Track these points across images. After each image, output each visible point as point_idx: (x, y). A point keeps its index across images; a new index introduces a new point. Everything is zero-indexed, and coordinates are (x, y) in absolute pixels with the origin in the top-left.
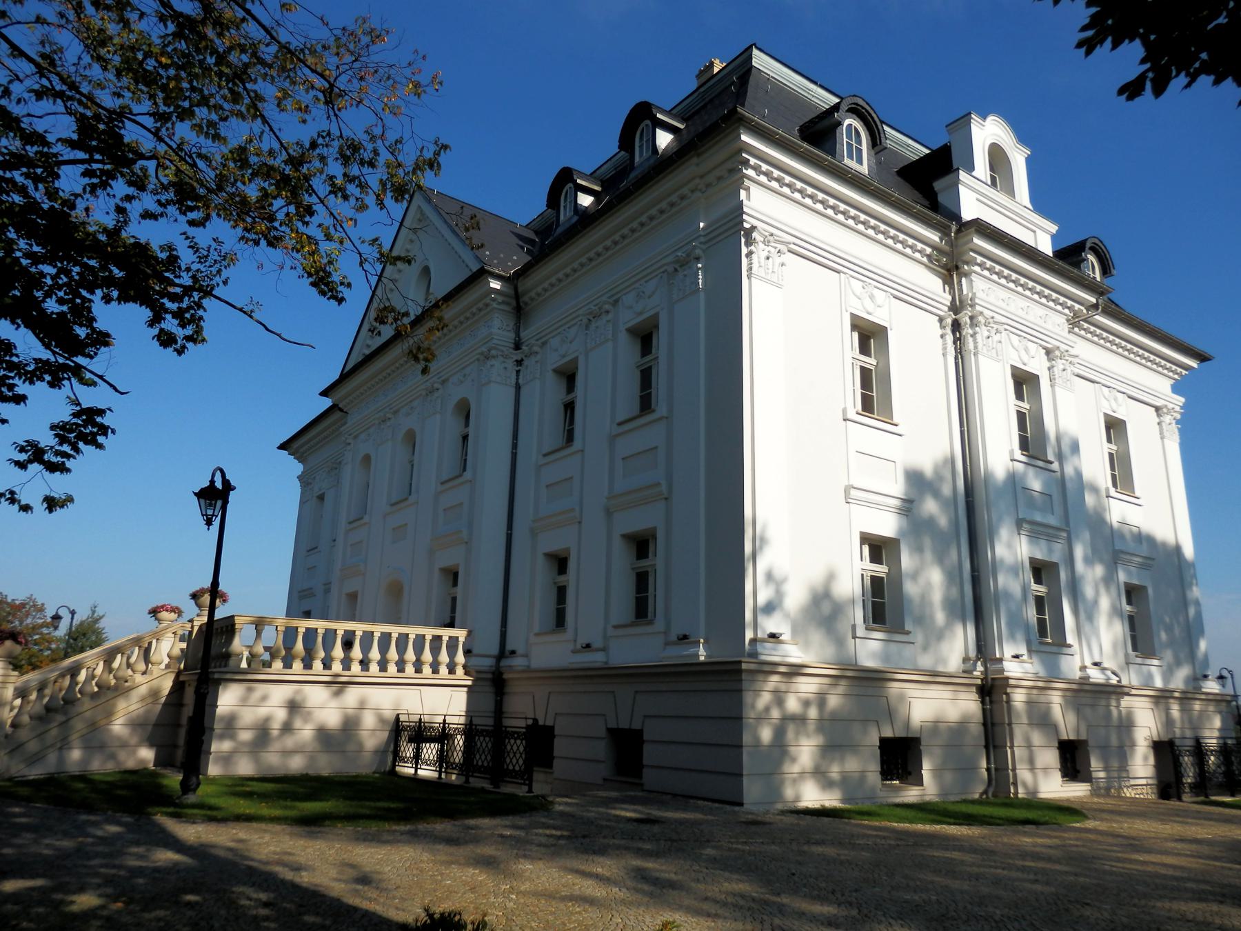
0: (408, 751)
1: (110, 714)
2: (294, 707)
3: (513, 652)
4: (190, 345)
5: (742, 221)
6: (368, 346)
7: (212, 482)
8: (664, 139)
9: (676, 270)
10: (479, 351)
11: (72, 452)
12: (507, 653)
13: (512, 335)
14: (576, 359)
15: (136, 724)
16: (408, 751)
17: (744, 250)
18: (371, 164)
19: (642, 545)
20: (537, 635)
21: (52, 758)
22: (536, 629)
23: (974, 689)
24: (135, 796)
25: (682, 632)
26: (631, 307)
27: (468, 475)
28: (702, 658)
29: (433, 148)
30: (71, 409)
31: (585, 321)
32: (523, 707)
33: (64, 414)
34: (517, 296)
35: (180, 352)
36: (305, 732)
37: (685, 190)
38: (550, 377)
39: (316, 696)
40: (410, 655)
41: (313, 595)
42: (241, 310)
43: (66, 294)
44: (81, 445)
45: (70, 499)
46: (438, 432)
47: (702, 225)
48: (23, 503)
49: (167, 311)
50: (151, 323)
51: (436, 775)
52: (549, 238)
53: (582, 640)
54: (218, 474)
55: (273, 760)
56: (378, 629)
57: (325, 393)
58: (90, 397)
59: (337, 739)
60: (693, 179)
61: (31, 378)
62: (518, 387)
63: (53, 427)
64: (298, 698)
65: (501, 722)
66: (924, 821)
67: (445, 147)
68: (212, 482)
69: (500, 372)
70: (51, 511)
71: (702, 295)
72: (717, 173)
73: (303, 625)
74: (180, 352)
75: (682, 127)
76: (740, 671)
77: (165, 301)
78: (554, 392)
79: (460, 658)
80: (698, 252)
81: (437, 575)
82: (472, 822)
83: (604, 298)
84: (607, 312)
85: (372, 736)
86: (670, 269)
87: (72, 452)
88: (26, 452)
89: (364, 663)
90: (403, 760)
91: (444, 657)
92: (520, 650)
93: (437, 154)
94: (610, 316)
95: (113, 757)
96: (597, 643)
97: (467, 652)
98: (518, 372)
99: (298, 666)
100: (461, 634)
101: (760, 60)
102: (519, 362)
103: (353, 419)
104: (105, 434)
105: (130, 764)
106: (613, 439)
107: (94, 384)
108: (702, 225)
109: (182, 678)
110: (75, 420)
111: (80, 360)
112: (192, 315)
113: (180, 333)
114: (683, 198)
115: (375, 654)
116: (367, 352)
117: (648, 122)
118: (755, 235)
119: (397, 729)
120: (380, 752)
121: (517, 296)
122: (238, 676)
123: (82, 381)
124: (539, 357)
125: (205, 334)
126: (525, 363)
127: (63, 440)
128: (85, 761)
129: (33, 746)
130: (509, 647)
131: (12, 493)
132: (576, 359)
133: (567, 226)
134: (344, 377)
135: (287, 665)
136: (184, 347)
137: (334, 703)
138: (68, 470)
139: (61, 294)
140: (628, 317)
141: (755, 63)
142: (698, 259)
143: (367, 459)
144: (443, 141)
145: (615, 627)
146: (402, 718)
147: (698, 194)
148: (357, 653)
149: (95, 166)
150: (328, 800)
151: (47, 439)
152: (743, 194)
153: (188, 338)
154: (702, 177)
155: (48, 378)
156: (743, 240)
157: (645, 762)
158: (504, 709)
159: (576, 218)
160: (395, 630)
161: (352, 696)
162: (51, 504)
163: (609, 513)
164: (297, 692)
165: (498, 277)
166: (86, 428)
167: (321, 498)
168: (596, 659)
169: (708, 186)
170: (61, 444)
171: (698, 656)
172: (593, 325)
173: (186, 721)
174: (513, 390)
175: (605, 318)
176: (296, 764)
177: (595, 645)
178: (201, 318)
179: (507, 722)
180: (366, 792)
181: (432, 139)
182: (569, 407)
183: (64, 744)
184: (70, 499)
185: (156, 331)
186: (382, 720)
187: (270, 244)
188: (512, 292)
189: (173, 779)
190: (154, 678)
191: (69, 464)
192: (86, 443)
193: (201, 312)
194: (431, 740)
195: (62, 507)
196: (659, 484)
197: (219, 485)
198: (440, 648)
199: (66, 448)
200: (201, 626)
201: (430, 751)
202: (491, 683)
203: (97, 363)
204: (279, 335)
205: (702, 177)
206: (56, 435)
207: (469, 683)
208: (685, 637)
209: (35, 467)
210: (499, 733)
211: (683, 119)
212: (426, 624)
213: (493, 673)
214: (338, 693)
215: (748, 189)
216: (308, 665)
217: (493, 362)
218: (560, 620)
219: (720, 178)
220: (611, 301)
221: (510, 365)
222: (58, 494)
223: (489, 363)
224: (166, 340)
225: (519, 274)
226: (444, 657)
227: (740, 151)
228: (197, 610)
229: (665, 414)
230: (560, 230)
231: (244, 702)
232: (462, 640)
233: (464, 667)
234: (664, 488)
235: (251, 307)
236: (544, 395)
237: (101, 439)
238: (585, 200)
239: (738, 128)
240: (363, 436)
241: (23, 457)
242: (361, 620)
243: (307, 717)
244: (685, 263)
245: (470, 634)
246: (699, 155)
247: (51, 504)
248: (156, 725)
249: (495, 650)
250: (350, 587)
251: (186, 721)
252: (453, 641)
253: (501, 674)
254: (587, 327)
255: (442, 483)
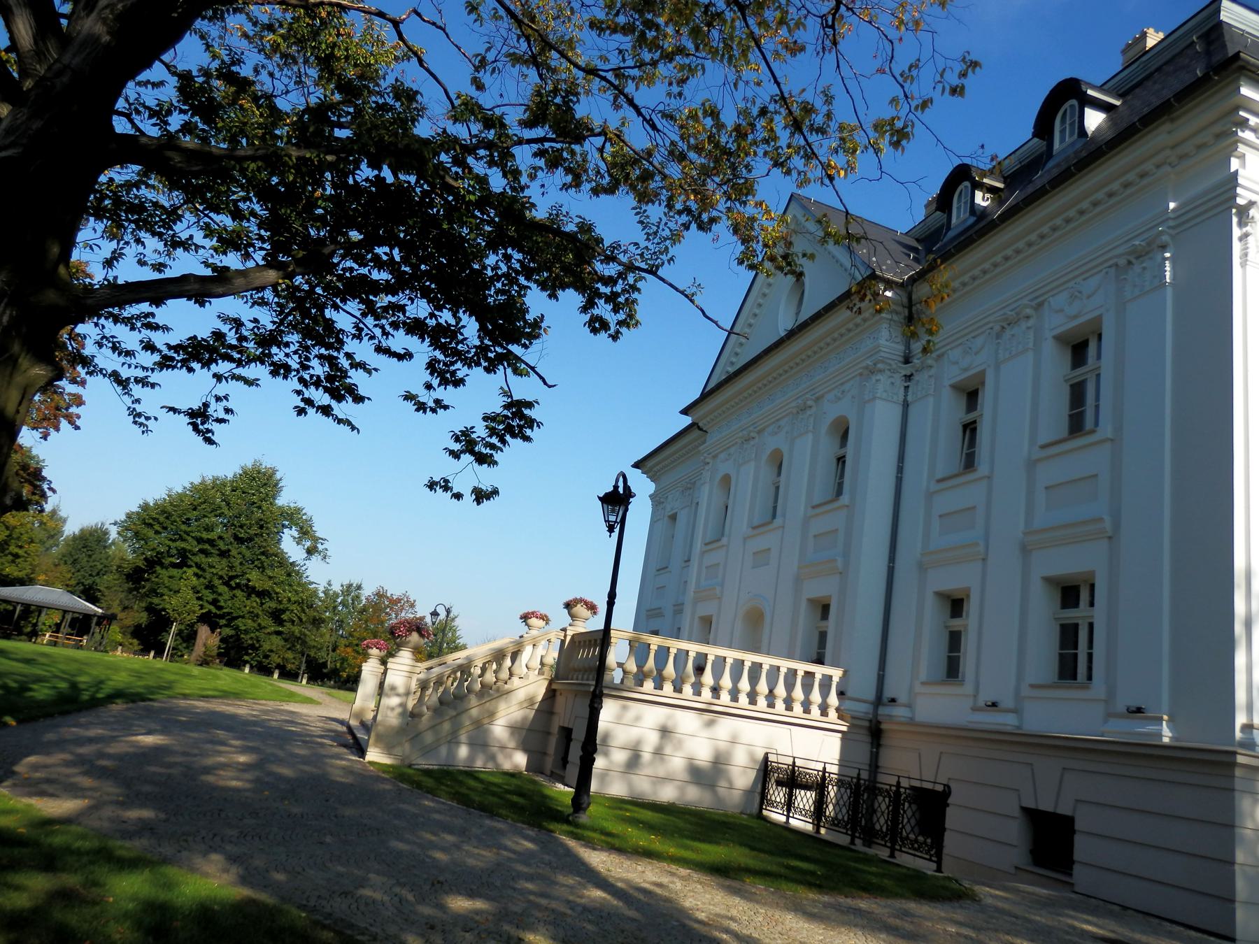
0: (778, 795)
1: (492, 715)
2: (665, 731)
3: (893, 700)
4: (624, 330)
5: (1235, 196)
6: (732, 363)
7: (616, 487)
8: (1094, 120)
9: (1130, 263)
10: (864, 364)
11: (499, 444)
12: (885, 700)
13: (902, 348)
14: (983, 373)
15: (514, 729)
16: (778, 795)
17: (1236, 232)
18: (821, 131)
19: (1069, 593)
20: (923, 683)
21: (443, 751)
22: (923, 676)
23: (840, 735)
24: (520, 804)
25: (1134, 704)
26: (1061, 310)
27: (845, 499)
28: (1166, 740)
29: (959, 67)
30: (502, 400)
31: (997, 328)
32: (906, 765)
33: (496, 405)
34: (910, 305)
35: (615, 337)
36: (677, 763)
37: (1148, 166)
38: (947, 395)
39: (687, 722)
40: (763, 687)
41: (661, 615)
42: (682, 293)
43: (503, 285)
44: (508, 438)
45: (495, 492)
46: (808, 456)
47: (1172, 205)
48: (455, 491)
49: (600, 296)
50: (584, 309)
51: (809, 827)
52: (942, 240)
53: (985, 697)
54: (621, 479)
55: (643, 786)
56: (731, 655)
57: (685, 412)
58: (523, 388)
59: (708, 775)
60: (1163, 149)
61: (469, 363)
62: (906, 405)
63: (486, 418)
64: (670, 724)
65: (875, 777)
66: (1043, 886)
67: (975, 64)
68: (616, 487)
69: (886, 387)
70: (479, 503)
71: (1169, 291)
72: (1199, 140)
73: (655, 642)
74: (615, 337)
75: (1117, 103)
76: (1234, 764)
77: (599, 285)
78: (952, 411)
79: (833, 700)
80: (1165, 238)
81: (804, 605)
82: (912, 906)
83: (1025, 301)
84: (1028, 317)
85: (742, 777)
86: (1122, 262)
87: (499, 444)
88: (460, 442)
89: (716, 690)
90: (771, 803)
91: (816, 696)
92: (902, 698)
93: (963, 75)
94: (1031, 323)
95: (492, 758)
96: (1007, 702)
97: (841, 694)
98: (907, 388)
99: (668, 688)
100: (836, 674)
101: (1232, 14)
102: (909, 377)
103: (713, 438)
104: (531, 428)
105: (507, 766)
106: (1032, 465)
107: (527, 374)
108: (1172, 205)
109: (554, 687)
110: (506, 412)
111: (515, 349)
112: (627, 299)
113: (612, 319)
114: (1143, 176)
115: (726, 682)
116: (731, 370)
117: (1074, 102)
118: (1252, 212)
119: (766, 769)
120: (748, 793)
121: (910, 305)
122: (618, 692)
123: (517, 372)
124: (932, 372)
125: (638, 317)
126: (916, 378)
127: (493, 432)
128: (471, 758)
129: (429, 738)
130: (888, 694)
131: (446, 481)
132: (983, 373)
133: (961, 229)
134: (705, 396)
135: (659, 687)
136: (618, 332)
137: (706, 733)
138: (495, 463)
139: (499, 285)
140: (1058, 321)
141: (1224, 17)
142: (1164, 248)
143: (726, 480)
144: (973, 57)
145: (1032, 686)
146: (772, 758)
147: (1167, 169)
148: (708, 678)
149: (547, 145)
150: (717, 843)
151: (481, 431)
152: (1235, 164)
153: (620, 323)
154: (1173, 147)
155: (485, 364)
156: (1235, 220)
157: (1076, 857)
158: (880, 764)
159: (973, 219)
160: (750, 658)
161: (726, 727)
162: (481, 496)
163: (1025, 550)
164: (669, 717)
165: (889, 284)
166: (515, 421)
167: (673, 518)
168: (1007, 721)
169: (1182, 157)
170: (491, 436)
171: (1160, 736)
172: (1008, 333)
173: (565, 730)
174: (898, 410)
175: (1024, 325)
176: (667, 794)
177: (1002, 705)
178: (634, 301)
179: (882, 778)
180: (733, 834)
181: (959, 55)
182: (970, 429)
183: (454, 741)
184: (495, 492)
185: (587, 317)
186: (753, 760)
187: (701, 227)
188: (905, 300)
189: (563, 791)
190: (529, 684)
191: (497, 456)
192: (514, 436)
193: (635, 295)
194: (807, 787)
195: (488, 499)
196: (1101, 520)
197: (621, 490)
198: (812, 686)
199: (494, 440)
200: (573, 636)
201: (805, 799)
202: (868, 733)
203: (529, 355)
204: (716, 323)
205: (1173, 147)
206: (487, 427)
207: (845, 729)
208: (1139, 710)
209: (466, 458)
210: (873, 788)
211: (1120, 96)
212: (790, 656)
213: (870, 721)
214: (710, 724)
215: (1242, 157)
216: (678, 689)
217: (879, 377)
218: (953, 670)
219: (1200, 147)
220: (1033, 303)
221: (900, 383)
222: (486, 486)
223: (874, 378)
224: (598, 325)
225: (913, 280)
226: (816, 696)
227: (1237, 108)
228: (569, 620)
229: (1109, 435)
230: (951, 234)
231: (618, 720)
232: (836, 680)
233: (837, 710)
234: (1108, 524)
235: (694, 289)
236: (938, 414)
237: (528, 432)
238: (981, 199)
239: (1238, 79)
240: (722, 456)
241: (457, 447)
242: (715, 644)
243: (679, 745)
244: (1146, 252)
245: (845, 673)
246: (1172, 120)
247: (481, 496)
248: (529, 730)
249: (871, 695)
250: (704, 610)
251: (565, 730)
252: (826, 682)
253: (879, 723)
254: (998, 336)
255: (813, 507)
